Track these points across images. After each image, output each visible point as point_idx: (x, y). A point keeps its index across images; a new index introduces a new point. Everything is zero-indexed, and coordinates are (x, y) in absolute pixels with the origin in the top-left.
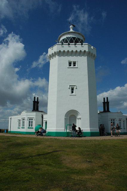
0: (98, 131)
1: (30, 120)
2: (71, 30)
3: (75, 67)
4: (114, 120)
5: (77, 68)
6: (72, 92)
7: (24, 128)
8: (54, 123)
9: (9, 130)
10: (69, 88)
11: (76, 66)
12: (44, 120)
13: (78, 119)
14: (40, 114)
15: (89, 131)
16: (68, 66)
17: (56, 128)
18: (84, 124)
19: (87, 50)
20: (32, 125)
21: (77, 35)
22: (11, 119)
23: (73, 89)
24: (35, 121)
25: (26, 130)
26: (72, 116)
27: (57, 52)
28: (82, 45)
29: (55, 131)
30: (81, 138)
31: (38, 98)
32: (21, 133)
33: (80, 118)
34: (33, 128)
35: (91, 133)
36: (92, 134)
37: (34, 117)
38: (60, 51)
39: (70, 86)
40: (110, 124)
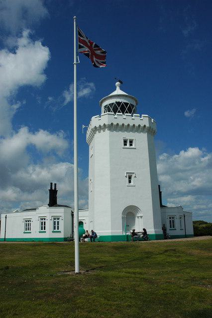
0: (193, 233)
1: (55, 219)
4: (173, 218)
5: (135, 149)
6: (130, 182)
7: (45, 232)
8: (102, 221)
10: (126, 177)
11: (133, 146)
13: (138, 217)
15: (154, 233)
16: (123, 146)
17: (112, 230)
18: (145, 223)
19: (147, 125)
20: (58, 227)
21: (131, 100)
22: (6, 217)
24: (63, 221)
26: (130, 214)
27: (109, 125)
29: (110, 235)
30: (166, 241)
31: (55, 184)
33: (141, 217)
34: (60, 232)
35: (64, 238)
36: (158, 237)
38: (112, 124)
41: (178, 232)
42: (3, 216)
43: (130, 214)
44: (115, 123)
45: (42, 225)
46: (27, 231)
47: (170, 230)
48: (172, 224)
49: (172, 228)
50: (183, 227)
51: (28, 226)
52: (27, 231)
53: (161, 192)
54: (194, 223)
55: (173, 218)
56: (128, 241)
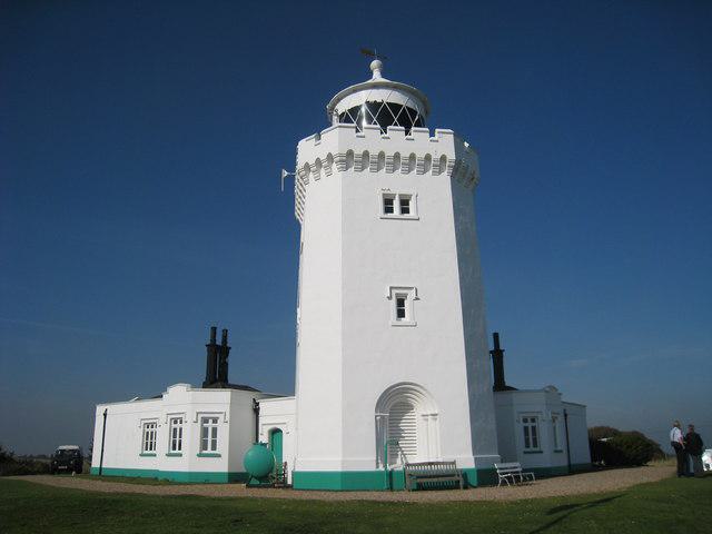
2: (377, 77)
3: (406, 216)
6: (401, 314)
7: (181, 455)
8: (319, 433)
9: (95, 463)
10: (390, 298)
12: (261, 421)
14: (247, 397)
18: (442, 436)
19: (451, 156)
20: (214, 443)
22: (105, 415)
23: (401, 302)
24: (228, 425)
25: (188, 462)
26: (394, 406)
28: (432, 134)
32: (605, 497)
36: (486, 477)
37: (227, 409)
38: (350, 153)
39: (391, 288)
40: (519, 428)
41: (546, 460)
42: (100, 410)
43: (394, 406)
44: (358, 151)
45: (175, 437)
46: (149, 452)
47: (525, 453)
48: (531, 436)
49: (532, 448)
50: (561, 446)
51: (149, 444)
52: (149, 452)
53: (502, 351)
54: (590, 431)
55: (533, 420)
56: (391, 489)
